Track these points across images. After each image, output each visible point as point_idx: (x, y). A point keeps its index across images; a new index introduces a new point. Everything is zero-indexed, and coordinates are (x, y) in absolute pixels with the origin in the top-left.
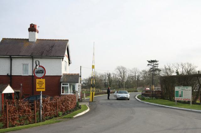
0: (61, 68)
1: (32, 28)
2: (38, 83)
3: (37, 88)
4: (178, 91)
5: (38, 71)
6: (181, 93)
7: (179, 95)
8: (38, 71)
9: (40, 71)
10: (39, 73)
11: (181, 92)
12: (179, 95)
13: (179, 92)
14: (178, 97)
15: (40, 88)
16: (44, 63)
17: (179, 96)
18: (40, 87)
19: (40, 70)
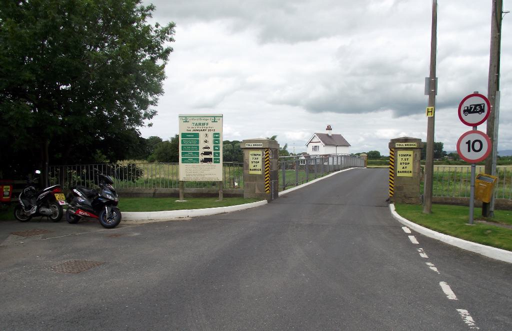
0: (299, 189)
1: (329, 128)
2: (408, 163)
3: (399, 172)
4: (197, 135)
5: (471, 108)
6: (211, 145)
7: (201, 151)
8: (471, 108)
9: (475, 108)
10: (474, 112)
11: (211, 139)
12: (201, 151)
13: (202, 138)
14: (197, 161)
15: (403, 172)
16: (409, 85)
17: (202, 157)
18: (403, 168)
19: (476, 106)
